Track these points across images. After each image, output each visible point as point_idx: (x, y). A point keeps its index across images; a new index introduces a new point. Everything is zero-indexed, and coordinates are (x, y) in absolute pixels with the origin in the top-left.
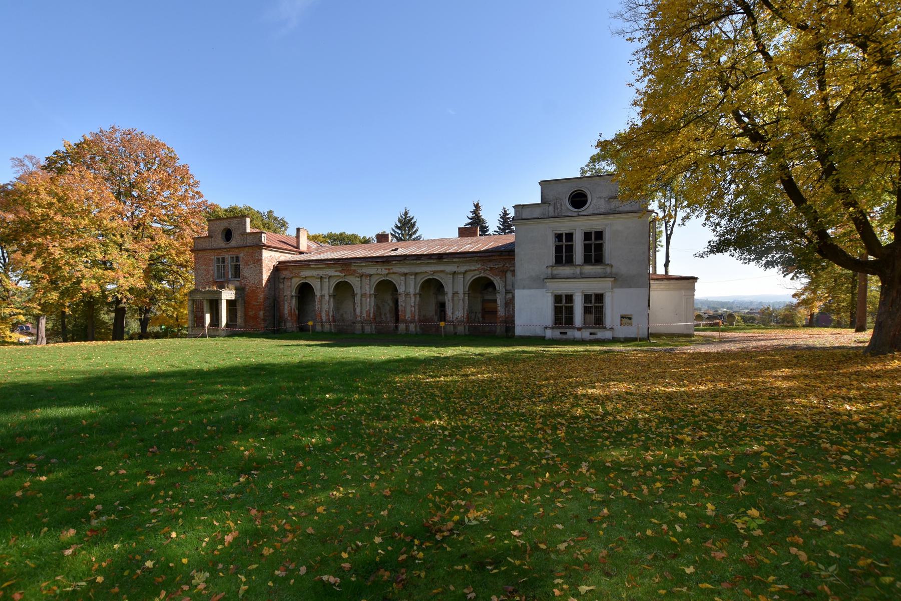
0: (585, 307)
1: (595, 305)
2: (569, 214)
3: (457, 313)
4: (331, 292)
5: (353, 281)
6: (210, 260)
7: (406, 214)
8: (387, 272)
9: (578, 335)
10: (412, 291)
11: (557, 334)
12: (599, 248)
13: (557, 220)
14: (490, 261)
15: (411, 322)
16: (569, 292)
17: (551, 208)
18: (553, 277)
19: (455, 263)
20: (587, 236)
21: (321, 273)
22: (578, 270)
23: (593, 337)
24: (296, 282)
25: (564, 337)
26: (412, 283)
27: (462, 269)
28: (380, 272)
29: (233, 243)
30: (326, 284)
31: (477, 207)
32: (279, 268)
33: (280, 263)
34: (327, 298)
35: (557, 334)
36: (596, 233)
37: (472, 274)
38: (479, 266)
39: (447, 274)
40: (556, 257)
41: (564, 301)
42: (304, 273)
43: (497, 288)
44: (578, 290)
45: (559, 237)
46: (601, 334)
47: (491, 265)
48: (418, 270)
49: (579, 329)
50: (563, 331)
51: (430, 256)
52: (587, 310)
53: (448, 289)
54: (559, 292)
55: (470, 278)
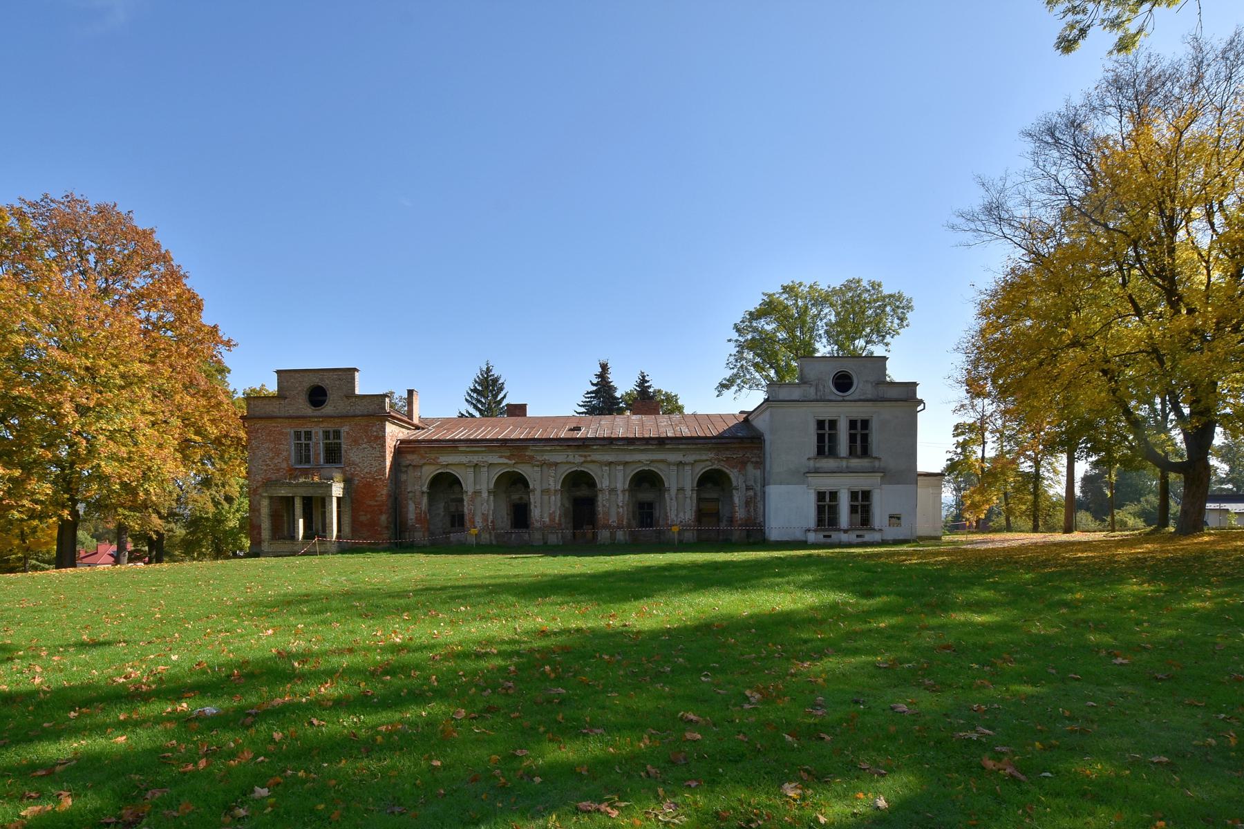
0: (852, 506)
1: (862, 503)
2: (833, 398)
3: (681, 515)
4: (492, 486)
5: (530, 473)
6: (282, 434)
7: (488, 370)
8: (582, 459)
9: (844, 537)
10: (620, 486)
11: (819, 537)
12: (865, 438)
13: (821, 404)
14: (727, 449)
15: (618, 527)
16: (833, 489)
17: (812, 390)
18: (816, 471)
19: (680, 450)
20: (853, 424)
21: (475, 459)
22: (844, 463)
23: (860, 540)
24: (429, 472)
25: (829, 540)
26: (620, 475)
27: (690, 458)
28: (574, 460)
29: (328, 409)
31: (604, 367)
32: (403, 448)
33: (402, 442)
34: (485, 495)
35: (819, 537)
36: (862, 421)
37: (703, 465)
38: (711, 455)
39: (669, 464)
40: (850, 448)
42: (445, 459)
43: (734, 484)
44: (844, 486)
45: (821, 424)
46: (868, 537)
47: (728, 454)
48: (628, 458)
49: (846, 531)
51: (647, 441)
52: (853, 510)
53: (468, 484)
54: (823, 489)
55: (700, 470)
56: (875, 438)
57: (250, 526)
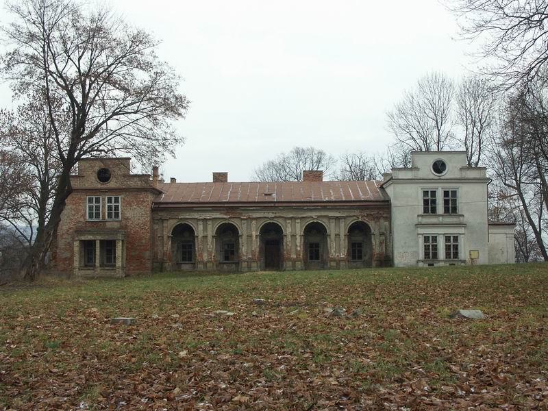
26: (298, 226)
29: (112, 184)
30: (210, 227)
37: (352, 219)
41: (94, 199)
45: (426, 193)
50: (431, 262)
55: (350, 222)
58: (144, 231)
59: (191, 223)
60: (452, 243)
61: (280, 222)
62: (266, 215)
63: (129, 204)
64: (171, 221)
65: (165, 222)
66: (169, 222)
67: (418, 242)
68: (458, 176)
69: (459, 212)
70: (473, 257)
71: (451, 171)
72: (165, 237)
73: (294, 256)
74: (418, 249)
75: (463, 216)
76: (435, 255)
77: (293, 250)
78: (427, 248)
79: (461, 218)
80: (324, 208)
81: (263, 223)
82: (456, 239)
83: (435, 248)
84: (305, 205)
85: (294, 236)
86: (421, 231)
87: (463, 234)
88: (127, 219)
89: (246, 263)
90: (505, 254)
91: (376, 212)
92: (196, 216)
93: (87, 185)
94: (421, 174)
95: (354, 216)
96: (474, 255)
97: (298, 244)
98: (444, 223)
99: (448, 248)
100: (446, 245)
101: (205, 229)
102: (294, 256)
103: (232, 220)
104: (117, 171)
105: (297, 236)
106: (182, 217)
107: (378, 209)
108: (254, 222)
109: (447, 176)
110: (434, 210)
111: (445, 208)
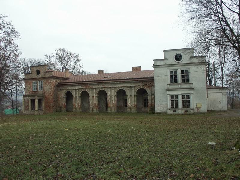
26: (113, 91)
30: (78, 92)
33: (59, 83)
37: (138, 87)
45: (171, 72)
50: (174, 110)
55: (137, 89)
56: (191, 77)
57: (137, 107)
58: (50, 95)
59: (71, 91)
60: (174, 99)
61: (105, 90)
62: (99, 86)
63: (46, 83)
64: (64, 90)
65: (62, 91)
66: (64, 91)
67: (167, 99)
68: (189, 62)
69: (190, 82)
70: (198, 107)
71: (185, 59)
72: (62, 97)
73: (112, 106)
74: (168, 102)
75: (192, 84)
76: (177, 106)
77: (111, 103)
78: (172, 102)
79: (191, 85)
80: (129, 82)
81: (98, 90)
82: (188, 97)
83: (177, 102)
84: (116, 81)
85: (111, 96)
86: (169, 93)
87: (192, 94)
88: (45, 90)
89: (92, 109)
90: (222, 103)
91: (149, 83)
92: (73, 88)
93: (33, 77)
94: (168, 62)
95: (139, 86)
96: (199, 106)
97: (113, 100)
98: (181, 88)
99: (184, 101)
100: (171, 101)
101: (76, 94)
102: (112, 106)
103: (86, 89)
104: (42, 70)
105: (113, 96)
106: (68, 88)
107: (150, 81)
108: (94, 90)
109: (183, 62)
110: (176, 81)
111: (182, 80)
